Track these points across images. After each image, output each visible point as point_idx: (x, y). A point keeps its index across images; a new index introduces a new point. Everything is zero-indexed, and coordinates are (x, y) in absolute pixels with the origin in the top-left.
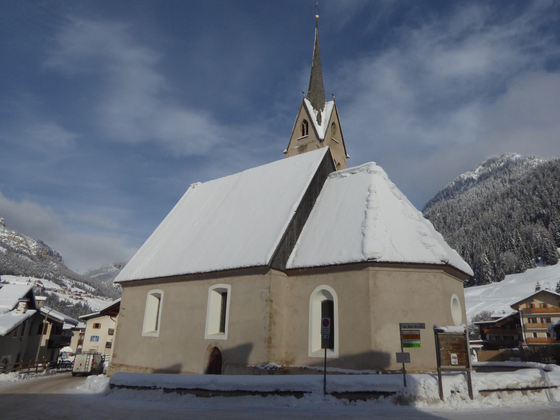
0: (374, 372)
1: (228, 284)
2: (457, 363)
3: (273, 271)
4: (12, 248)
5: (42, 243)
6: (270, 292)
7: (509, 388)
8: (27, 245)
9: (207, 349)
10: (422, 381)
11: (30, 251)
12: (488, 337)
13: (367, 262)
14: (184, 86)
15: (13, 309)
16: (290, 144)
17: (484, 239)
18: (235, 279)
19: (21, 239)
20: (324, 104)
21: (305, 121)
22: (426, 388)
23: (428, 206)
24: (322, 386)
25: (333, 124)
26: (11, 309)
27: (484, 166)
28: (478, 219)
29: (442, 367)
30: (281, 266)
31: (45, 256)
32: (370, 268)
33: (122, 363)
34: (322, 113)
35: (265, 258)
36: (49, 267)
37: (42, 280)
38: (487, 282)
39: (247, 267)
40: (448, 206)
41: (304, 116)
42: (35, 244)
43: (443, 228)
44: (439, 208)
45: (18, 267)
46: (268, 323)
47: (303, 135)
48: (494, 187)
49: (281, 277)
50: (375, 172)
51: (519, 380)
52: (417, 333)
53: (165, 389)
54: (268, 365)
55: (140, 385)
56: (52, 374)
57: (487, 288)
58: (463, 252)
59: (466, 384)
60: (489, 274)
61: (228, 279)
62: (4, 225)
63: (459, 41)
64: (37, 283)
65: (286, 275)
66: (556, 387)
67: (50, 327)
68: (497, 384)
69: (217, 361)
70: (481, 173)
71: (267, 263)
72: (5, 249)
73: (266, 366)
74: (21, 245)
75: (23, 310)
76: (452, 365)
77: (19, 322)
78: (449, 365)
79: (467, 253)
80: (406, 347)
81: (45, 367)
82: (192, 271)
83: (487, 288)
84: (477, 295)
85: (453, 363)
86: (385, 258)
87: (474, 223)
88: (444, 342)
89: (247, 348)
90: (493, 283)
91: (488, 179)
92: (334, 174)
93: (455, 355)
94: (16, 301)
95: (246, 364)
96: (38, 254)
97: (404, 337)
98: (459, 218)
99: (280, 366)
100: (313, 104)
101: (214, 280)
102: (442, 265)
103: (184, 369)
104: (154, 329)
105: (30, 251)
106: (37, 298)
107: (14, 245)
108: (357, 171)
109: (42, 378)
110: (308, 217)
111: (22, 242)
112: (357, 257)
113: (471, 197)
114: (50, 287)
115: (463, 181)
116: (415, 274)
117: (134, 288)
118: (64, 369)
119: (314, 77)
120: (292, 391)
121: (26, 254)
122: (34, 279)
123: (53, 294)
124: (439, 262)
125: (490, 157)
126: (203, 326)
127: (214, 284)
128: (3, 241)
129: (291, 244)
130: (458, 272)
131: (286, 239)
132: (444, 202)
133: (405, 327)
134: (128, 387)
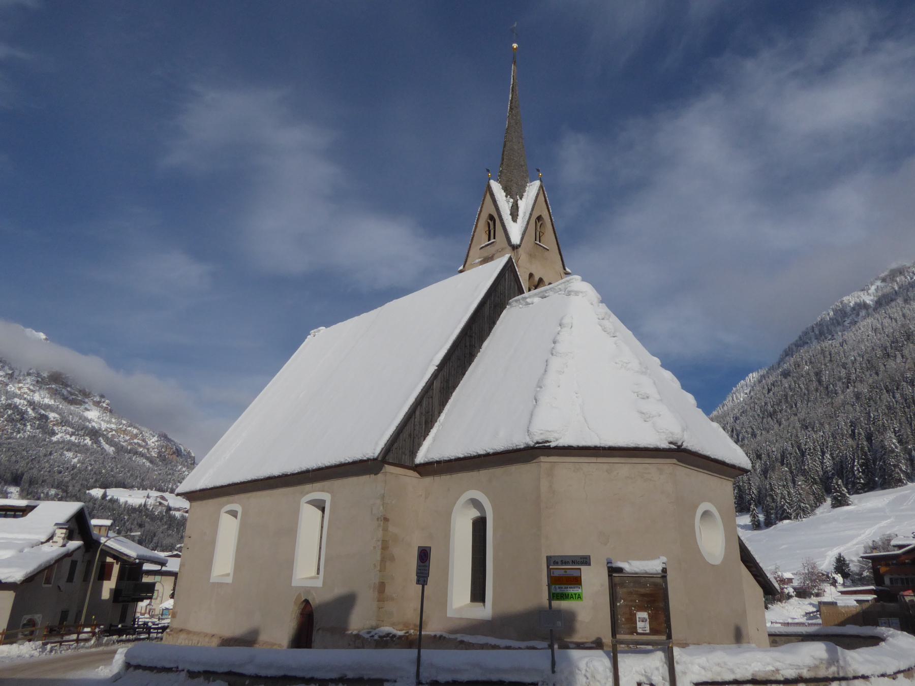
0: (545, 644)
1: (328, 492)
2: (648, 631)
3: (388, 468)
4: (123, 447)
5: (165, 437)
6: (383, 505)
7: (758, 678)
8: (144, 440)
9: (295, 603)
10: (582, 664)
11: (148, 449)
12: (887, 581)
13: (533, 448)
14: (373, 179)
15: (48, 541)
16: (468, 256)
17: (889, 408)
18: (338, 484)
19: (135, 431)
20: (525, 187)
21: (491, 217)
22: (588, 675)
23: (787, 355)
24: (413, 670)
25: (539, 218)
26: (43, 540)
27: (884, 280)
28: (877, 374)
29: (618, 636)
30: (406, 460)
31: (171, 457)
32: (542, 459)
33: (181, 627)
34: (519, 202)
35: (373, 448)
36: (177, 474)
37: (166, 495)
38: (899, 482)
39: (349, 464)
40: (823, 352)
41: (489, 209)
42: (156, 439)
43: (817, 390)
44: (806, 357)
45: (132, 475)
46: (379, 558)
47: (489, 240)
48: (904, 316)
49: (410, 478)
50: (577, 293)
51: (778, 665)
52: (575, 574)
53: (188, 671)
54: (377, 631)
55: (159, 665)
56: (107, 644)
57: (898, 494)
58: (853, 431)
59: (665, 670)
60: (901, 469)
61: (327, 484)
62: (111, 411)
63: (826, 70)
64: (159, 500)
65: (417, 475)
66: (865, 677)
67: (116, 569)
68: (732, 671)
69: (310, 625)
70: (880, 294)
71: (376, 455)
72: (113, 448)
73: (372, 633)
74: (136, 441)
75: (61, 542)
76: (638, 634)
77: (48, 561)
78: (632, 633)
79: (859, 434)
80: (558, 599)
81: (94, 634)
82: (276, 472)
83: (898, 494)
84: (880, 505)
85: (640, 631)
86: (564, 441)
87: (871, 381)
88: (625, 590)
89: (346, 602)
90: (910, 484)
91: (893, 304)
92: (516, 301)
93: (644, 615)
94: (50, 529)
95: (346, 629)
96: (160, 454)
97: (554, 580)
98: (843, 373)
99: (401, 633)
100: (506, 189)
101: (308, 487)
102: (670, 450)
103: (263, 637)
104: (313, 573)
105: (148, 449)
106: (94, 522)
107: (126, 441)
108: (551, 293)
109: (88, 651)
110: (464, 374)
111: (136, 436)
112: (520, 440)
113: (864, 334)
114: (177, 506)
115: (848, 308)
116: (624, 468)
117: (205, 502)
118: (131, 637)
119: (508, 144)
120: (366, 677)
121: (142, 455)
122: (154, 494)
123: (183, 516)
124: (664, 445)
125: (894, 266)
126: (289, 564)
127: (307, 493)
128: (110, 435)
129: (426, 422)
130: (712, 463)
131: (418, 413)
132: (816, 346)
133: (556, 563)
134: (145, 668)
